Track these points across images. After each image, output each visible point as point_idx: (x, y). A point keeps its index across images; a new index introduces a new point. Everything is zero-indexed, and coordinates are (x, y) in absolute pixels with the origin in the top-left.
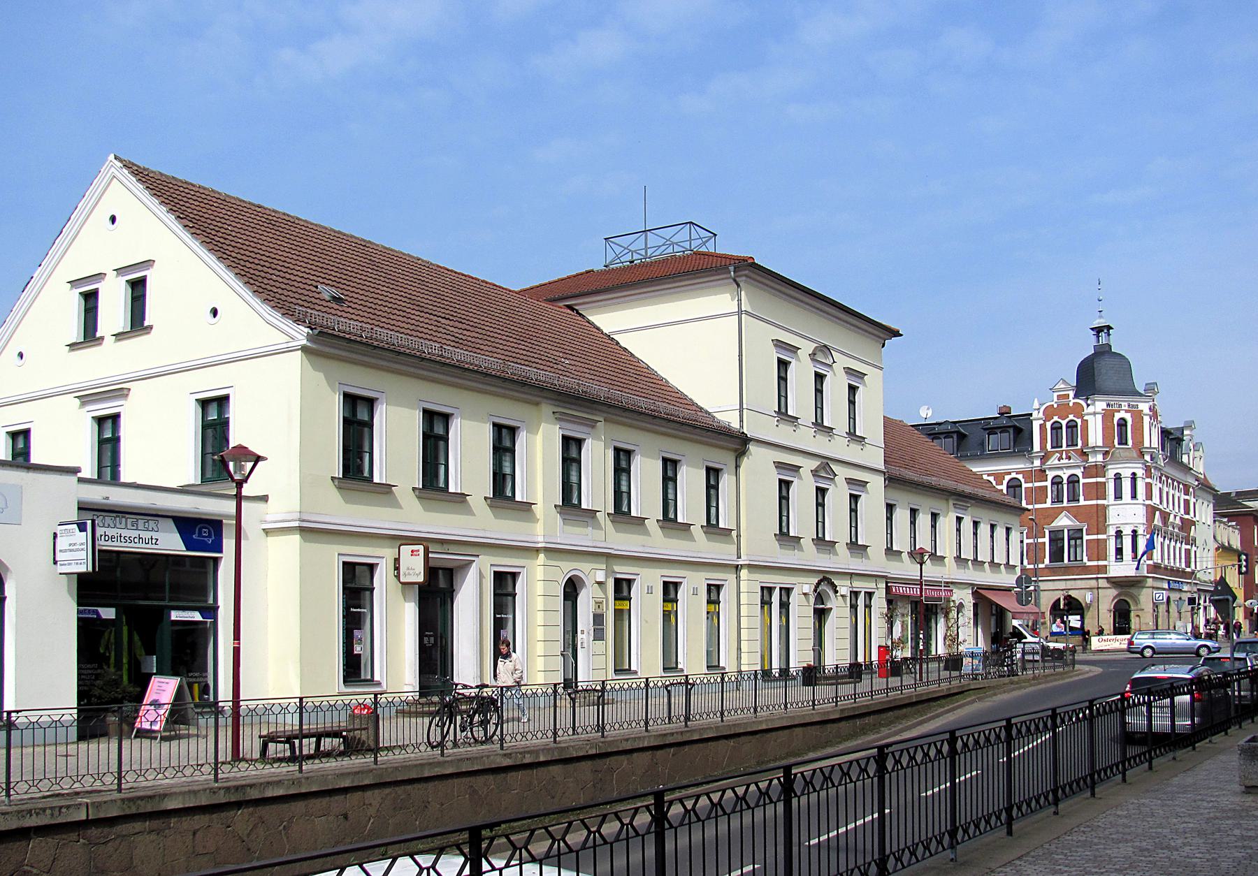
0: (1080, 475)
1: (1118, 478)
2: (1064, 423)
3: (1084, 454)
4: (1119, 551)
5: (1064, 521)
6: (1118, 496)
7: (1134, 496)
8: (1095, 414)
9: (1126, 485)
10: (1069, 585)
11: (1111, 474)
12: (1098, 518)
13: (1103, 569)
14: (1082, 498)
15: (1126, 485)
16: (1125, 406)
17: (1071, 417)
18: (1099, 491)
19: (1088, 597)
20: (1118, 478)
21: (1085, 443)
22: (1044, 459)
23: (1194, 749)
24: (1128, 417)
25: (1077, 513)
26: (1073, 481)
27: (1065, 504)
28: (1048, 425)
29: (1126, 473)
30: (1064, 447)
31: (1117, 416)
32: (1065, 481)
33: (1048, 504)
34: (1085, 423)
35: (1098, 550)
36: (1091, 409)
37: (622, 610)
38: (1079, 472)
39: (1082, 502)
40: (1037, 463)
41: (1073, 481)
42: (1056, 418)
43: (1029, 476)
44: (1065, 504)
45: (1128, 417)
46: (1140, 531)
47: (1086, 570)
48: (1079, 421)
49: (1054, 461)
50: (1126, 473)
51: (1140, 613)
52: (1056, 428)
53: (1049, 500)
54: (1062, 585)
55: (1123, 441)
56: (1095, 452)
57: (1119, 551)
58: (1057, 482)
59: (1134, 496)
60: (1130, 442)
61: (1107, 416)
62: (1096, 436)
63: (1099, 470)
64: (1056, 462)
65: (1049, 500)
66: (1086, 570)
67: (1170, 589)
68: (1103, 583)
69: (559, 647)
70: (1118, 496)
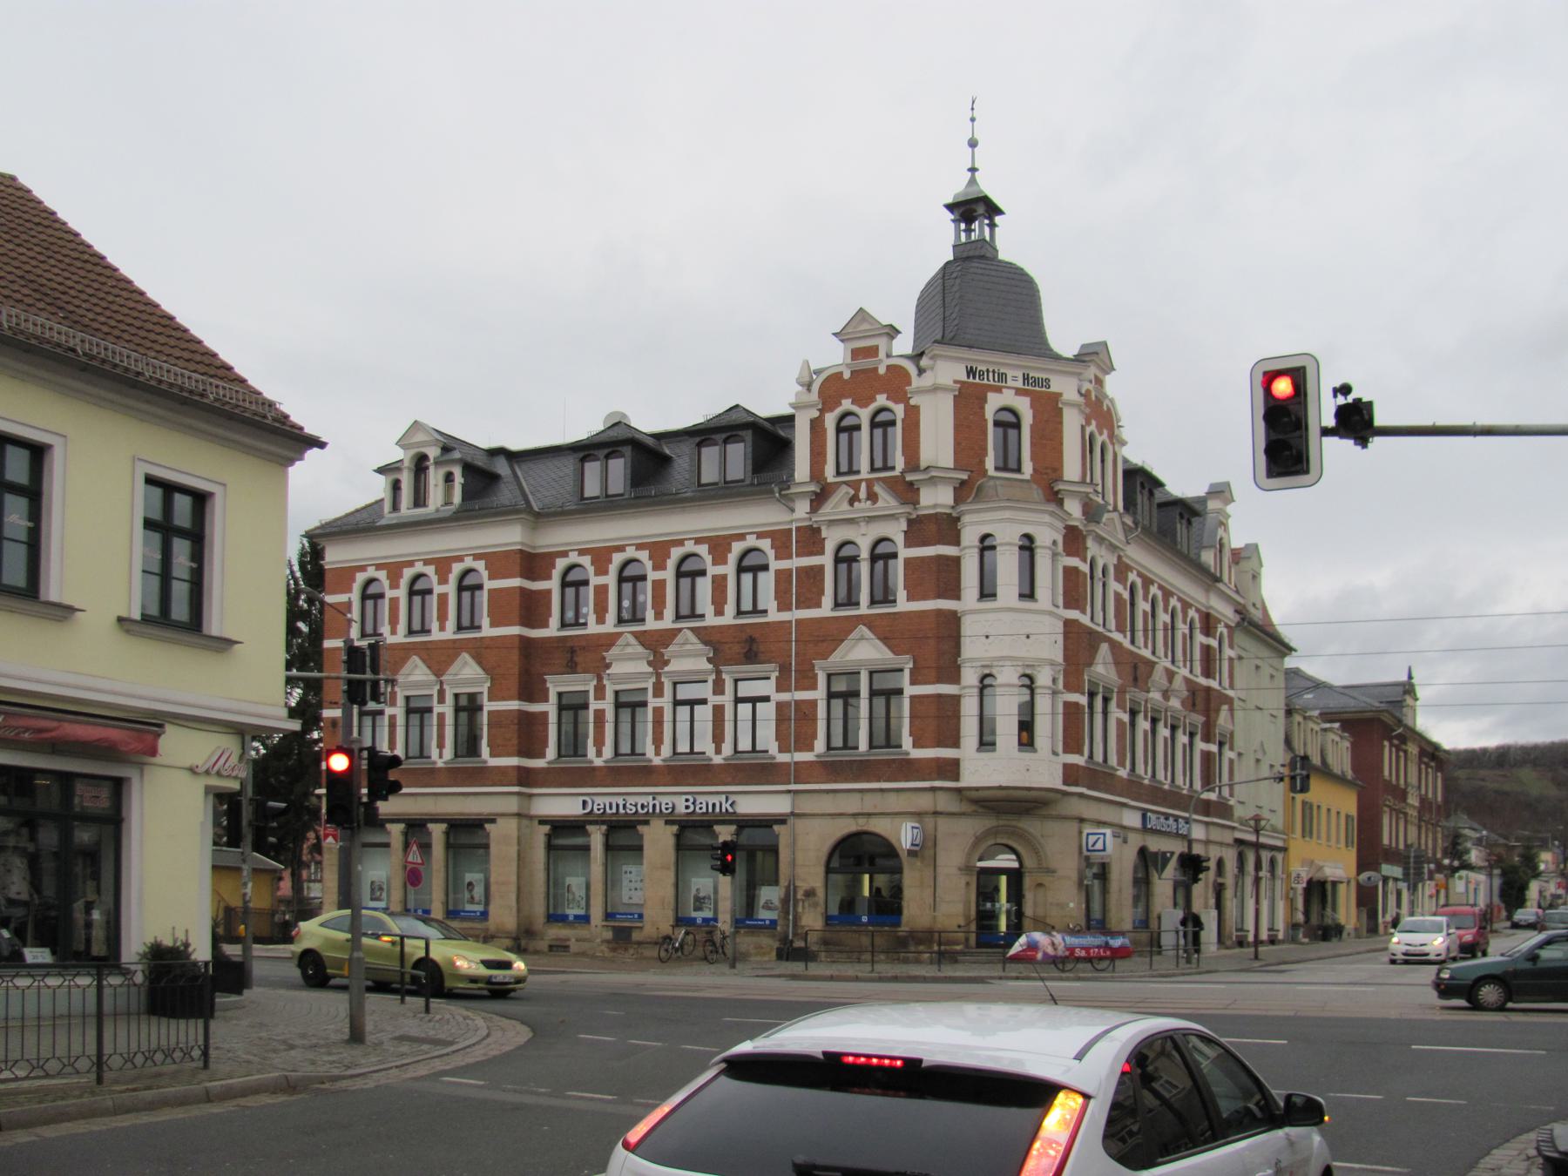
0: (899, 539)
1: (986, 545)
2: (865, 415)
3: (907, 491)
4: (1026, 727)
5: (864, 651)
6: (987, 592)
7: (1029, 594)
8: (935, 389)
9: (1007, 566)
10: (869, 804)
11: (970, 536)
12: (939, 645)
13: (951, 769)
14: (901, 594)
15: (1007, 566)
16: (1015, 378)
17: (881, 400)
18: (944, 577)
19: (905, 836)
20: (986, 545)
21: (913, 464)
22: (819, 498)
23: (403, 1001)
24: (1023, 406)
25: (891, 632)
26: (881, 556)
27: (864, 609)
28: (830, 420)
29: (1007, 533)
30: (865, 473)
31: (994, 402)
32: (865, 554)
33: (826, 609)
34: (913, 414)
35: (940, 721)
36: (927, 380)
37: (362, 683)
38: (896, 531)
39: (903, 604)
40: (802, 508)
41: (881, 556)
42: (847, 404)
43: (781, 541)
44: (864, 609)
45: (1023, 406)
46: (1043, 678)
47: (908, 769)
48: (899, 410)
49: (836, 506)
50: (1007, 533)
51: (1046, 879)
52: (846, 429)
53: (827, 600)
54: (852, 804)
55: (1009, 463)
56: (933, 481)
57: (1026, 727)
58: (845, 560)
59: (1029, 594)
60: (1028, 468)
61: (968, 399)
62: (938, 443)
63: (946, 527)
64: (845, 506)
65: (827, 600)
66: (908, 769)
67: (1145, 829)
68: (945, 803)
69: (156, 568)
70: (987, 592)
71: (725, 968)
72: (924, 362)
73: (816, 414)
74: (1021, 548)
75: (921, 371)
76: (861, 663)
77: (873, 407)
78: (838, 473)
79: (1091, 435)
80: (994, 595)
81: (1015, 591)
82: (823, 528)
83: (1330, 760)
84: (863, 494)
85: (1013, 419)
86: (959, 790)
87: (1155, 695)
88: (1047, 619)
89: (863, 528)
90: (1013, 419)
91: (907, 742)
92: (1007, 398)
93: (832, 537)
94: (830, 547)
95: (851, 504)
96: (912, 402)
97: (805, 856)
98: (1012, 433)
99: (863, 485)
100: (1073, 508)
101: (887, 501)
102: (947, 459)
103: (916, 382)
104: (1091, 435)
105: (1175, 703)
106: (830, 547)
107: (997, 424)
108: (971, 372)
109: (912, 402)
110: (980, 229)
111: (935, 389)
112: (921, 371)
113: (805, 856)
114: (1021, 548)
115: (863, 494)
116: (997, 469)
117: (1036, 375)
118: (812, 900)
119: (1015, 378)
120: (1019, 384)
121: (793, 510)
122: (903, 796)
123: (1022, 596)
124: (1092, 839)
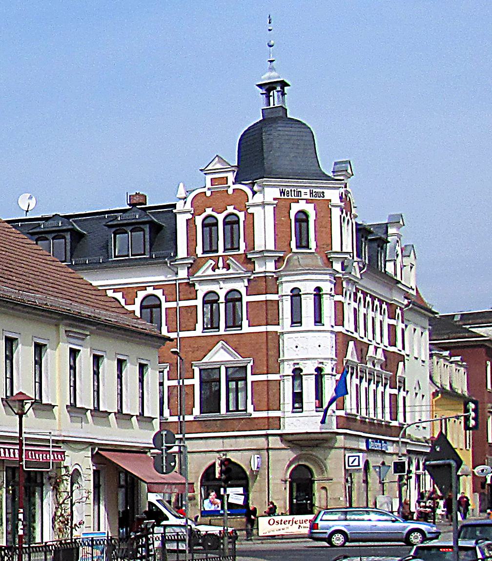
0: (243, 291)
1: (296, 294)
2: (220, 218)
5: (220, 355)
6: (296, 320)
7: (318, 320)
8: (263, 205)
9: (308, 305)
11: (286, 289)
15: (308, 305)
16: (305, 193)
18: (270, 312)
20: (296, 294)
21: (250, 246)
24: (310, 209)
25: (237, 344)
26: (233, 299)
27: (222, 331)
28: (199, 220)
29: (307, 288)
31: (295, 208)
32: (222, 299)
35: (269, 396)
36: (258, 198)
38: (241, 286)
40: (183, 273)
41: (233, 299)
42: (209, 211)
44: (222, 331)
45: (310, 209)
46: (327, 369)
48: (241, 215)
49: (206, 270)
50: (307, 288)
52: (210, 225)
54: (217, 445)
55: (303, 244)
58: (210, 300)
59: (318, 320)
60: (313, 244)
61: (281, 207)
62: (265, 236)
63: (270, 284)
64: (210, 272)
66: (252, 423)
67: (369, 451)
68: (275, 442)
70: (296, 320)
71: (416, 499)
72: (256, 188)
73: (190, 216)
74: (315, 295)
75: (254, 193)
76: (222, 363)
77: (225, 213)
78: (204, 252)
79: (344, 217)
80: (301, 322)
81: (312, 320)
82: (197, 284)
83: (454, 386)
84: (221, 264)
85: (304, 217)
86: (280, 435)
87: (370, 365)
88: (329, 334)
89: (222, 284)
90: (304, 217)
91: (250, 408)
92: (302, 206)
93: (202, 290)
94: (200, 295)
95: (214, 270)
96: (250, 211)
97: (411, 475)
98: (304, 225)
99: (221, 258)
100: (337, 266)
101: (237, 269)
102: (271, 246)
103: (251, 201)
104: (344, 217)
105: (378, 368)
106: (200, 295)
107: (296, 220)
108: (282, 192)
109: (250, 211)
110: (275, 99)
111: (263, 205)
112: (254, 193)
113: (411, 475)
114: (315, 295)
115: (221, 264)
116: (297, 247)
117: (317, 190)
118: (193, 502)
119: (306, 194)
120: (308, 197)
121: (177, 274)
122: (248, 440)
123: (316, 322)
124: (351, 459)
